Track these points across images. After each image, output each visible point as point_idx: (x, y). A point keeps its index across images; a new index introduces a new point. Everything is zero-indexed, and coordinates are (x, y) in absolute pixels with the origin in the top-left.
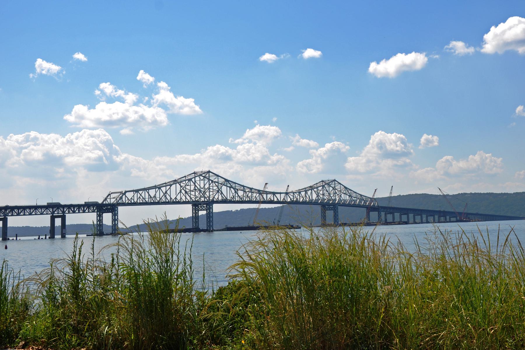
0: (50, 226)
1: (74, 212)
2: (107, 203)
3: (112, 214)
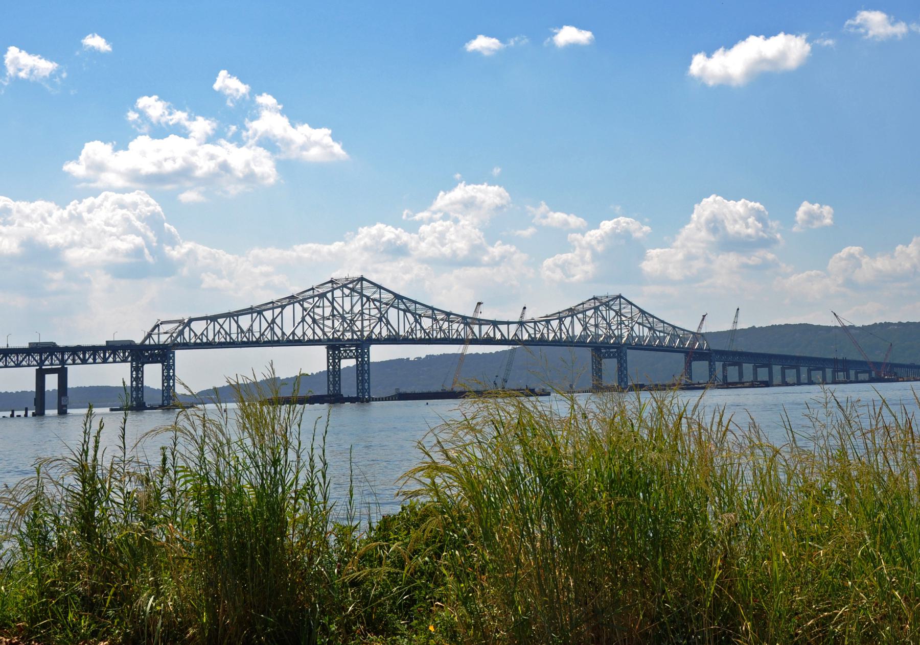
0: (34, 390)
1: (84, 362)
2: (152, 342)
3: (163, 365)
